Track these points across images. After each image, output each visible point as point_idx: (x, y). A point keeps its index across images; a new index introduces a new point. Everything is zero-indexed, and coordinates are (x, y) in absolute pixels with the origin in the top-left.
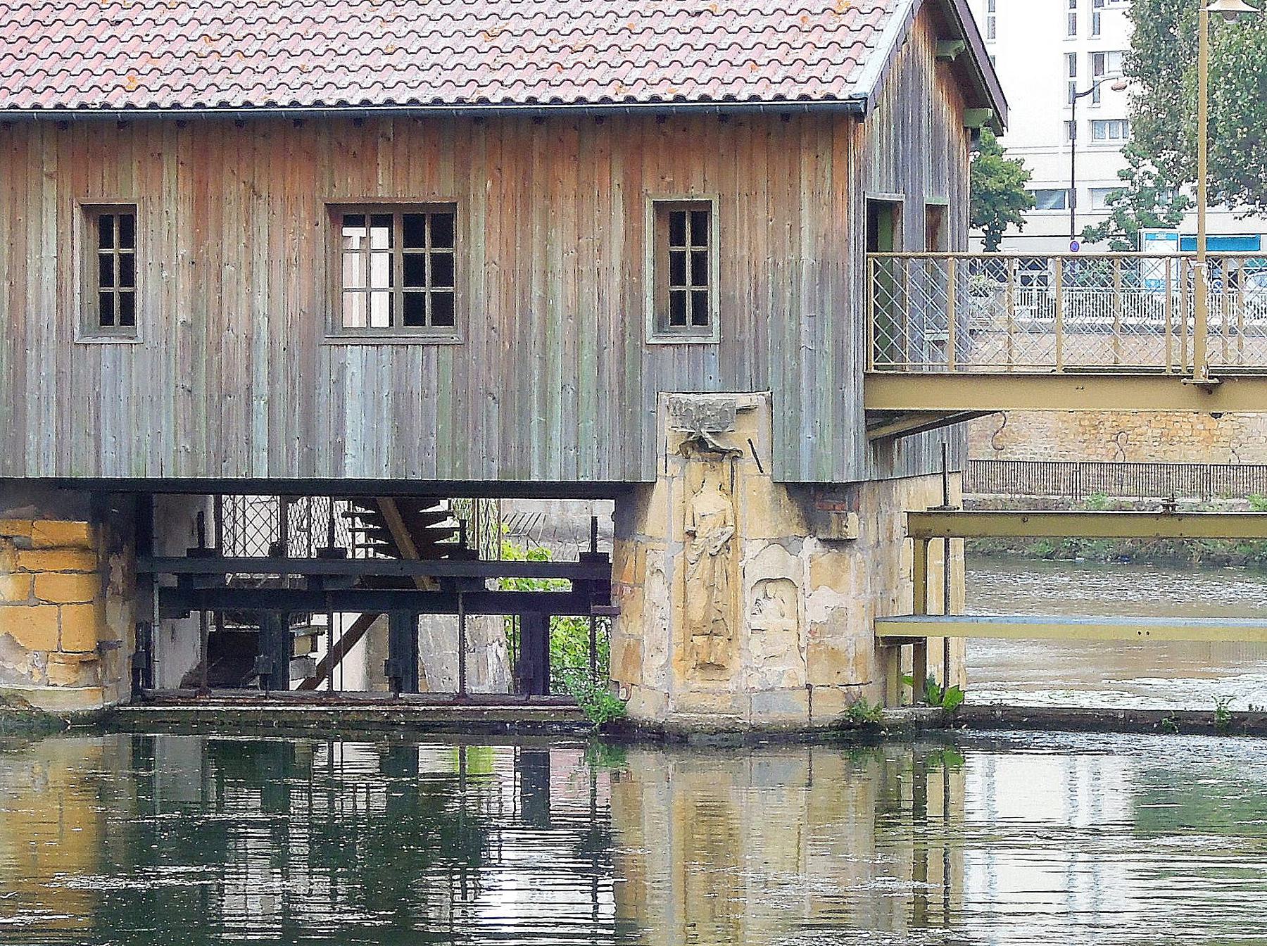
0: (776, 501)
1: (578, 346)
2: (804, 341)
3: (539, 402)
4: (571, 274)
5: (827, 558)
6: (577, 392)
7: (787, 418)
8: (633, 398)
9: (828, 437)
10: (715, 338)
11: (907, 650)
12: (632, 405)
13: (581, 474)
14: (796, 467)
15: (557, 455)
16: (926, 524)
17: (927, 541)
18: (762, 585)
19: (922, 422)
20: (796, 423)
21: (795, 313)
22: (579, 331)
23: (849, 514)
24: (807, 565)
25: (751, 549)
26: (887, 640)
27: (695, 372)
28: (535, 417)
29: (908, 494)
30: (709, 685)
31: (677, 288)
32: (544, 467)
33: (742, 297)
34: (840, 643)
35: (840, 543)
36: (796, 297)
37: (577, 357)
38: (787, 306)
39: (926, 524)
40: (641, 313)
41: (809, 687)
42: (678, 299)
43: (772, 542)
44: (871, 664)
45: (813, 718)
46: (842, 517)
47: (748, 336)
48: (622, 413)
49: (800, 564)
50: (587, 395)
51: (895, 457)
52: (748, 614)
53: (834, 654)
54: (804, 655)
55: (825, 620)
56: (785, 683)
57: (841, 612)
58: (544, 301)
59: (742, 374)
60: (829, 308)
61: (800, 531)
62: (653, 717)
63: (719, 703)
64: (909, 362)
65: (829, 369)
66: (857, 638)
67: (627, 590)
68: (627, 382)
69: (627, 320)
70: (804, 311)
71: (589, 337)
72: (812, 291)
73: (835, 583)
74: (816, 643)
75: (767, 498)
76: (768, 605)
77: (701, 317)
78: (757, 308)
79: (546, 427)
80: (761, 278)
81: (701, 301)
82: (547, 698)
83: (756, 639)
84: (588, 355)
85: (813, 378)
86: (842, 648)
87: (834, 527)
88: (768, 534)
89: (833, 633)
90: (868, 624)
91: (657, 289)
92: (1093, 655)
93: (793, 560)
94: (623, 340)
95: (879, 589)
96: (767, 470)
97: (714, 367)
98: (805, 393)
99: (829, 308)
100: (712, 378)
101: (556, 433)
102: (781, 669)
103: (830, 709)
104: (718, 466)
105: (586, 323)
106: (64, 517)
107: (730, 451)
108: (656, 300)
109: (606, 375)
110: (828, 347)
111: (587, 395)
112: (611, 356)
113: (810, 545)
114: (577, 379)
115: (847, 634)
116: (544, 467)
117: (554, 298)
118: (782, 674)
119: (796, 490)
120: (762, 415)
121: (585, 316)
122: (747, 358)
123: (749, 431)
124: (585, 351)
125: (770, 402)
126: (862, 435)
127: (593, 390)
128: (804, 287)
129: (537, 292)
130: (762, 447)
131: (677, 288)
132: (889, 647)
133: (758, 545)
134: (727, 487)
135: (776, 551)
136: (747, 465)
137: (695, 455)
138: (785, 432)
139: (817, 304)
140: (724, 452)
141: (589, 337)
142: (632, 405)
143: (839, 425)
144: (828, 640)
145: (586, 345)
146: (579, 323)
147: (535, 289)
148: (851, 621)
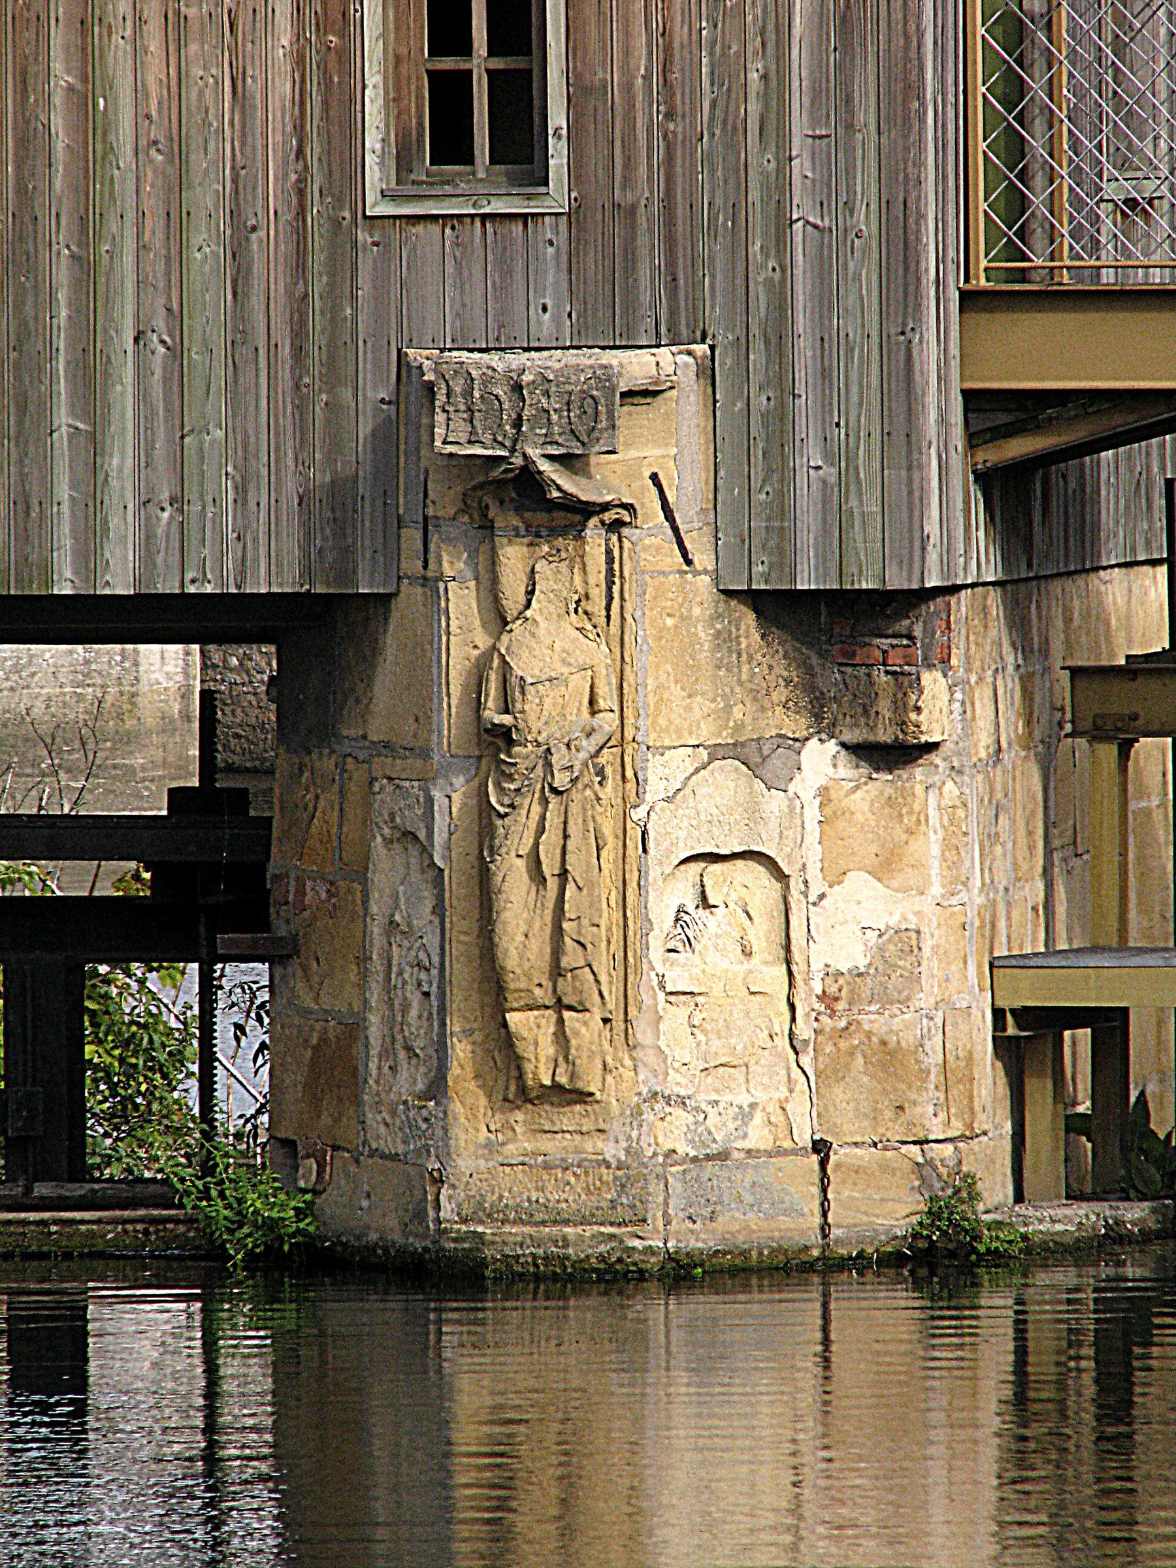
0: (725, 640)
1: (177, 222)
2: (802, 206)
3: (71, 378)
4: (154, 27)
5: (867, 794)
6: (176, 352)
7: (755, 417)
8: (331, 363)
9: (867, 461)
10: (558, 193)
11: (1078, 1043)
12: (332, 380)
13: (189, 576)
14: (784, 558)
15: (122, 523)
16: (1119, 700)
17: (1131, 743)
18: (695, 868)
19: (1121, 421)
20: (780, 423)
21: (775, 129)
22: (178, 183)
23: (927, 678)
24: (812, 813)
25: (663, 773)
26: (1023, 1015)
27: (503, 291)
28: (63, 418)
29: (1068, 620)
30: (548, 1145)
31: (448, 63)
32: (89, 555)
33: (628, 87)
34: (900, 1025)
35: (894, 754)
36: (776, 83)
37: (177, 257)
38: (754, 107)
39: (1119, 700)
40: (353, 132)
41: (821, 1148)
42: (449, 94)
43: (717, 753)
44: (989, 1080)
45: (835, 1233)
46: (906, 684)
47: (646, 190)
48: (301, 407)
49: (795, 808)
50: (207, 357)
51: (1037, 517)
52: (656, 954)
53: (889, 1058)
54: (806, 1060)
55: (862, 963)
56: (758, 1136)
57: (903, 943)
58: (81, 101)
59: (631, 293)
60: (866, 114)
61: (795, 725)
62: (397, 1237)
63: (568, 1194)
64: (1108, 253)
65: (869, 277)
66: (953, 1011)
67: (314, 892)
68: (317, 322)
69: (314, 150)
70: (799, 124)
71: (207, 195)
72: (819, 65)
73: (885, 867)
74: (838, 1027)
75: (704, 634)
76: (711, 924)
77: (519, 147)
78: (670, 115)
79: (93, 444)
80: (680, 33)
81: (518, 100)
82: (78, 1190)
83: (675, 1017)
84: (206, 248)
85: (824, 302)
86: (909, 1039)
87: (884, 706)
88: (707, 733)
89: (884, 999)
90: (974, 972)
91: (396, 63)
92: (46, 1440)
93: (775, 802)
94: (302, 211)
95: (1002, 881)
96: (703, 559)
97: (552, 278)
98: (804, 350)
99: (866, 114)
100: (548, 305)
101: (120, 461)
102: (744, 1099)
103: (885, 1211)
104: (567, 544)
105: (199, 162)
106: (372, 666)
107: (606, 507)
108: (395, 99)
109: (256, 302)
110: (865, 220)
111: (207, 357)
112: (269, 248)
113: (821, 760)
114: (176, 317)
115: (924, 1000)
116: (89, 555)
117: (109, 88)
118: (745, 1114)
119: (778, 609)
120: (687, 405)
121: (196, 141)
122: (643, 252)
123: (652, 452)
124: (198, 239)
125: (707, 372)
126: (956, 461)
127: (219, 343)
128: (799, 55)
129: (62, 75)
130: (689, 490)
131: (448, 63)
132: (1027, 1039)
133: (680, 762)
134: (597, 606)
135: (727, 779)
136: (649, 542)
137: (507, 520)
138: (753, 449)
139: (833, 96)
140: (587, 510)
141: (207, 195)
142: (332, 380)
143: (901, 439)
144: (873, 1020)
145: (199, 217)
146: (179, 155)
147: (57, 66)
148: (931, 965)
